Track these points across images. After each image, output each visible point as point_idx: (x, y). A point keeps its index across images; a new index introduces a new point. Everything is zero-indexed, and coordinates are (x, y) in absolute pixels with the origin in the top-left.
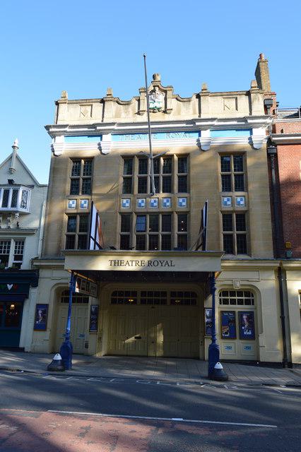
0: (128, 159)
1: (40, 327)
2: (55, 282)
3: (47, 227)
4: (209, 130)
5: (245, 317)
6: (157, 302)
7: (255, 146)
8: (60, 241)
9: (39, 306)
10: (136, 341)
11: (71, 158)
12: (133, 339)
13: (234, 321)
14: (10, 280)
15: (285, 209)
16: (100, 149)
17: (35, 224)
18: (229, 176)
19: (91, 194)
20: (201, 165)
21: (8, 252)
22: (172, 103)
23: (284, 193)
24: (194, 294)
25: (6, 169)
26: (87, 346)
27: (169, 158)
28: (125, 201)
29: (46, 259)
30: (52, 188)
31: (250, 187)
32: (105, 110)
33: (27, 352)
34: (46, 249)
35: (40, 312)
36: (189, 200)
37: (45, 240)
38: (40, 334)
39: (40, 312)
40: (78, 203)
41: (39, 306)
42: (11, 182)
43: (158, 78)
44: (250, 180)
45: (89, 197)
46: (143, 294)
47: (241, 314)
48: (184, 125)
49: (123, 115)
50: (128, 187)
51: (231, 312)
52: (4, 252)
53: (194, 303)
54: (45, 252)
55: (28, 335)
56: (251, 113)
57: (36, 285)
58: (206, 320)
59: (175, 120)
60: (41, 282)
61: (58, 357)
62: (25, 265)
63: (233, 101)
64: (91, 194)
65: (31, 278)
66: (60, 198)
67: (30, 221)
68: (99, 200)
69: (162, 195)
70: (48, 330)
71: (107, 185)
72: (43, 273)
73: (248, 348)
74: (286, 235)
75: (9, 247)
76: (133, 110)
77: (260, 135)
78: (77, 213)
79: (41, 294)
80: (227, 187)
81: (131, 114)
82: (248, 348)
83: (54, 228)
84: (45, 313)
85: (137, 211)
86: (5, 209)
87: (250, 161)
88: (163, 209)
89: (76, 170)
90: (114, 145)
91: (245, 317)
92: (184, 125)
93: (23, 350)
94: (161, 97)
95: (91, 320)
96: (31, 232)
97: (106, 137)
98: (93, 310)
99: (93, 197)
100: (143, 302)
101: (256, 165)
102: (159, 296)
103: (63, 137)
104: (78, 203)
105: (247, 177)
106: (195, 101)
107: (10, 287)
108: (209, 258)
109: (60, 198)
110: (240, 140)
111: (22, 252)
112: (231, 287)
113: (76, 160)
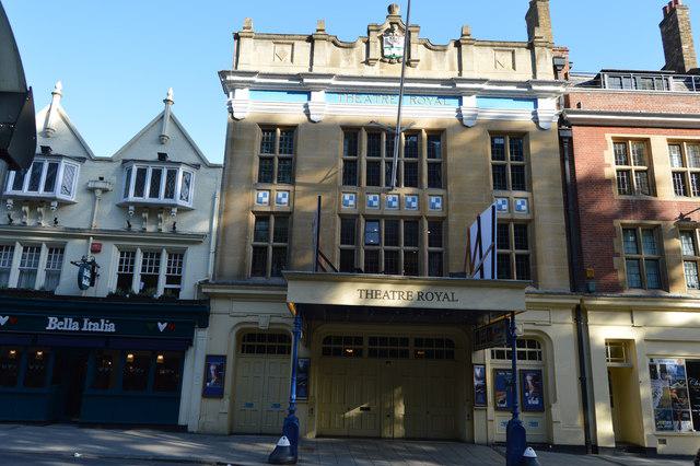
0: (351, 132)
1: (212, 391)
3: (223, 232)
5: (529, 378)
6: (394, 354)
7: (236, 115)
8: (244, 255)
9: (210, 359)
11: (261, 125)
12: (357, 411)
13: (514, 384)
16: (308, 113)
17: (202, 227)
18: (504, 166)
19: (292, 182)
20: (463, 147)
21: (157, 270)
24: (450, 343)
25: (154, 134)
28: (347, 197)
31: (536, 186)
34: (221, 266)
35: (212, 368)
36: (445, 200)
37: (219, 253)
38: (213, 403)
39: (212, 368)
41: (210, 359)
42: (162, 157)
44: (534, 174)
45: (291, 188)
49: (343, 63)
50: (350, 176)
53: (450, 355)
54: (218, 272)
55: (191, 402)
57: (204, 325)
59: (378, 75)
62: (187, 292)
64: (292, 182)
65: (197, 314)
67: (198, 220)
68: (305, 194)
69: (404, 191)
72: (216, 306)
75: (158, 263)
76: (359, 57)
77: (548, 109)
79: (215, 338)
80: (500, 182)
83: (234, 234)
84: (221, 370)
87: (534, 147)
89: (268, 144)
90: (329, 108)
91: (529, 378)
92: (286, 81)
94: (400, 40)
96: (197, 239)
97: (318, 97)
100: (373, 353)
101: (544, 153)
103: (246, 90)
106: (453, 50)
107: (162, 327)
108: (508, 290)
110: (519, 114)
113: (268, 128)
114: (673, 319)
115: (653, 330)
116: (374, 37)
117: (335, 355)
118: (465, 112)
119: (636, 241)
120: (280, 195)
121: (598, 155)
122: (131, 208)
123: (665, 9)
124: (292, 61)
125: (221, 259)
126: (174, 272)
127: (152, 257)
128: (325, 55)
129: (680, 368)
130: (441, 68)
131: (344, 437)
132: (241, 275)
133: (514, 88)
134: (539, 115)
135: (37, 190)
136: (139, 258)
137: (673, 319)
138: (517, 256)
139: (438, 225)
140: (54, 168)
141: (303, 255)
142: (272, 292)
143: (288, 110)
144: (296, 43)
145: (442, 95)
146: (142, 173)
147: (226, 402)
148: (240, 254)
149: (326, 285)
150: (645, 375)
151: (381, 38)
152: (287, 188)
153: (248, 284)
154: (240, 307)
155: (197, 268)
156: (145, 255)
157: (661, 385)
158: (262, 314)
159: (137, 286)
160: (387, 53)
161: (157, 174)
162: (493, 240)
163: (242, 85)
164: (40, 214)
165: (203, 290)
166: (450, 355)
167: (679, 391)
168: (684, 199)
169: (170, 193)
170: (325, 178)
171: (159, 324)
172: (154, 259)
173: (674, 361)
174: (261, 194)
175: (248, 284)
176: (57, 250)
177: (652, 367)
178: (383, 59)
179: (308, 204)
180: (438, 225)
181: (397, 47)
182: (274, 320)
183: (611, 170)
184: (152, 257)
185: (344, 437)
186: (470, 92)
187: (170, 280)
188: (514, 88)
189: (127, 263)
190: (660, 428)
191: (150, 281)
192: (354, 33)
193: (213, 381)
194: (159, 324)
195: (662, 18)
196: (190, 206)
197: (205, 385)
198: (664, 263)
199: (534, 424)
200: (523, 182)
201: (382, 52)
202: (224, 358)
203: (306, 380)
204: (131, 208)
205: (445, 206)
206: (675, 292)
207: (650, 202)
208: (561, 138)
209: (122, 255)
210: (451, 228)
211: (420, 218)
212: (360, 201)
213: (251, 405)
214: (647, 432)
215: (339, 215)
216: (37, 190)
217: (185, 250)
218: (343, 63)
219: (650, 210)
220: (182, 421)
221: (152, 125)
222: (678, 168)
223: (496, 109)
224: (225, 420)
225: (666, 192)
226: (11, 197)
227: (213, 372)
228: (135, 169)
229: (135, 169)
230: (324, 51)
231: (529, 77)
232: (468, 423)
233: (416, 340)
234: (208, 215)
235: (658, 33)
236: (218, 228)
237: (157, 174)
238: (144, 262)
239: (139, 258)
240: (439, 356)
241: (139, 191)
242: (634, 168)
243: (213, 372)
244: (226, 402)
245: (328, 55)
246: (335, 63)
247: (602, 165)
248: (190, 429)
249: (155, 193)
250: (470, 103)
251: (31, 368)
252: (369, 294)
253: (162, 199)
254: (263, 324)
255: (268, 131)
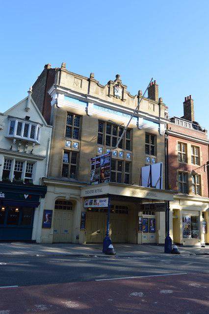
0: (101, 122)
1: (46, 226)
2: (57, 195)
3: (52, 157)
4: (93, 104)
5: (152, 221)
7: (88, 113)
8: (60, 170)
9: (45, 211)
10: (97, 235)
11: (68, 112)
12: (95, 233)
13: (148, 224)
14: (26, 191)
15: (169, 168)
16: (87, 111)
17: (44, 153)
19: (80, 140)
20: (138, 137)
21: (21, 170)
22: (126, 97)
23: (170, 160)
25: (23, 106)
26: (78, 238)
27: (122, 128)
28: (100, 149)
29: (70, 182)
30: (55, 129)
31: (158, 154)
32: (90, 86)
33: (140, 244)
34: (51, 172)
35: (47, 215)
36: (131, 155)
37: (50, 166)
38: (47, 231)
39: (47, 215)
40: (71, 144)
41: (45, 211)
42: (27, 118)
43: (120, 78)
44: (158, 150)
45: (79, 142)
46: (117, 207)
47: (151, 219)
48: (80, 96)
49: (100, 93)
50: (100, 141)
51: (44, 215)
52: (18, 170)
53: (127, 212)
54: (50, 174)
55: (38, 231)
56: (89, 93)
57: (43, 197)
58: (140, 223)
59: (112, 102)
60: (48, 195)
61: (111, 246)
62: (36, 181)
63: (80, 81)
64: (80, 140)
65: (41, 191)
66: (61, 138)
67: (41, 150)
68: (85, 145)
69: (119, 150)
70: (52, 227)
71: (90, 136)
72: (49, 189)
73: (152, 237)
74: (170, 181)
76: (106, 93)
77: (163, 128)
78: (71, 151)
79: (47, 203)
80: (147, 152)
81: (104, 95)
82: (152, 237)
83: (56, 158)
84: (50, 216)
85: (65, 148)
86: (11, 136)
87: (158, 141)
88: (73, 149)
89: (70, 121)
90: (95, 111)
91: (152, 221)
92: (80, 96)
93: (34, 242)
94: (120, 90)
95: (82, 221)
96: (40, 158)
97: (91, 105)
98: (83, 215)
99: (82, 142)
100: (117, 211)
101: (161, 143)
102: (64, 207)
103: (63, 95)
104: (71, 144)
105: (156, 149)
106: (136, 99)
107: (26, 196)
108: (169, 194)
109: (61, 138)
110: (154, 128)
111: (31, 171)
112: (64, 198)
113: (70, 114)
114: (189, 203)
115: (184, 206)
116: (112, 86)
117: (59, 209)
118: (140, 124)
119: (181, 177)
120: (75, 144)
121: (174, 147)
122: (15, 140)
123: (186, 98)
124: (81, 87)
125: (51, 168)
126: (29, 172)
127: (20, 163)
128: (94, 89)
129: (189, 219)
130: (132, 104)
131: (98, 243)
132: (58, 176)
133: (154, 118)
134: (88, 109)
135: (27, 137)
136: (14, 164)
137: (189, 203)
138: (71, 166)
139: (128, 164)
140: (33, 128)
141: (83, 170)
142: (67, 184)
143: (79, 108)
144: (83, 80)
145: (81, 100)
146: (20, 124)
147: (52, 229)
148: (57, 169)
149: (121, 188)
150: (181, 221)
151: (114, 87)
152: (78, 141)
153: (63, 181)
154: (58, 190)
155: (39, 173)
156: (16, 162)
157: (185, 224)
158: (67, 193)
159: (12, 177)
160: (116, 94)
161: (27, 126)
162: (161, 175)
163: (62, 93)
164: (20, 146)
165: (45, 181)
166: (127, 212)
167: (189, 226)
168: (194, 165)
169: (32, 137)
170: (92, 140)
171: (25, 195)
172: (18, 164)
173: (188, 217)
174: (67, 142)
175: (63, 181)
176: (30, 164)
177: (183, 218)
178: (114, 96)
179: (86, 149)
180: (128, 164)
181: (119, 93)
182: (72, 196)
183: (177, 153)
184: (20, 163)
185: (98, 243)
186: (141, 116)
187: (27, 175)
188: (154, 118)
189: (8, 165)
190: (184, 237)
191: (18, 175)
192: (104, 83)
193: (47, 221)
194: (25, 195)
195: (184, 101)
196: (39, 143)
197: (43, 222)
198: (188, 185)
199: (145, 237)
200: (101, 141)
201: (114, 93)
202: (52, 211)
203: (84, 221)
204: (15, 140)
205: (131, 158)
206: (190, 195)
207: (186, 165)
208: (165, 139)
209: (5, 161)
210: (133, 166)
211: (123, 161)
212: (104, 151)
213: (67, 231)
214: (181, 239)
215: (64, 149)
216: (27, 137)
217: (34, 163)
218: (100, 93)
219: (186, 168)
220: (33, 238)
221: (22, 102)
222: (193, 155)
223: (150, 125)
224: (51, 237)
225: (190, 162)
226: (15, 138)
227: (47, 217)
228: (17, 122)
229: (17, 122)
230: (94, 86)
231: (86, 92)
232: (136, 237)
233: (116, 206)
234: (46, 148)
235: (182, 105)
236: (50, 154)
237: (27, 126)
238: (16, 166)
239: (14, 164)
240: (123, 212)
241: (19, 133)
242: (73, 126)
243: (47, 217)
244: (52, 229)
245: (95, 88)
246: (97, 93)
247: (175, 151)
248: (37, 242)
249: (26, 135)
250: (141, 121)
251: (11, 216)
252: (133, 193)
253: (29, 138)
254: (67, 198)
255: (70, 115)
